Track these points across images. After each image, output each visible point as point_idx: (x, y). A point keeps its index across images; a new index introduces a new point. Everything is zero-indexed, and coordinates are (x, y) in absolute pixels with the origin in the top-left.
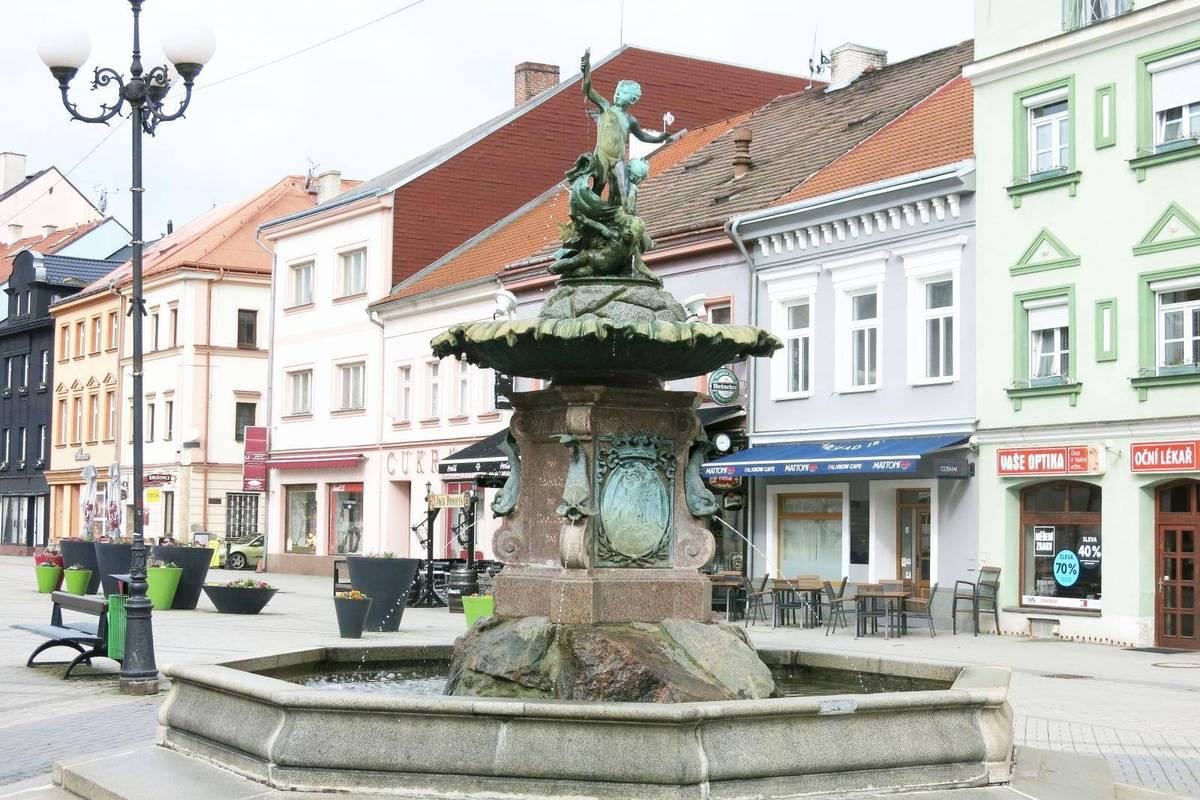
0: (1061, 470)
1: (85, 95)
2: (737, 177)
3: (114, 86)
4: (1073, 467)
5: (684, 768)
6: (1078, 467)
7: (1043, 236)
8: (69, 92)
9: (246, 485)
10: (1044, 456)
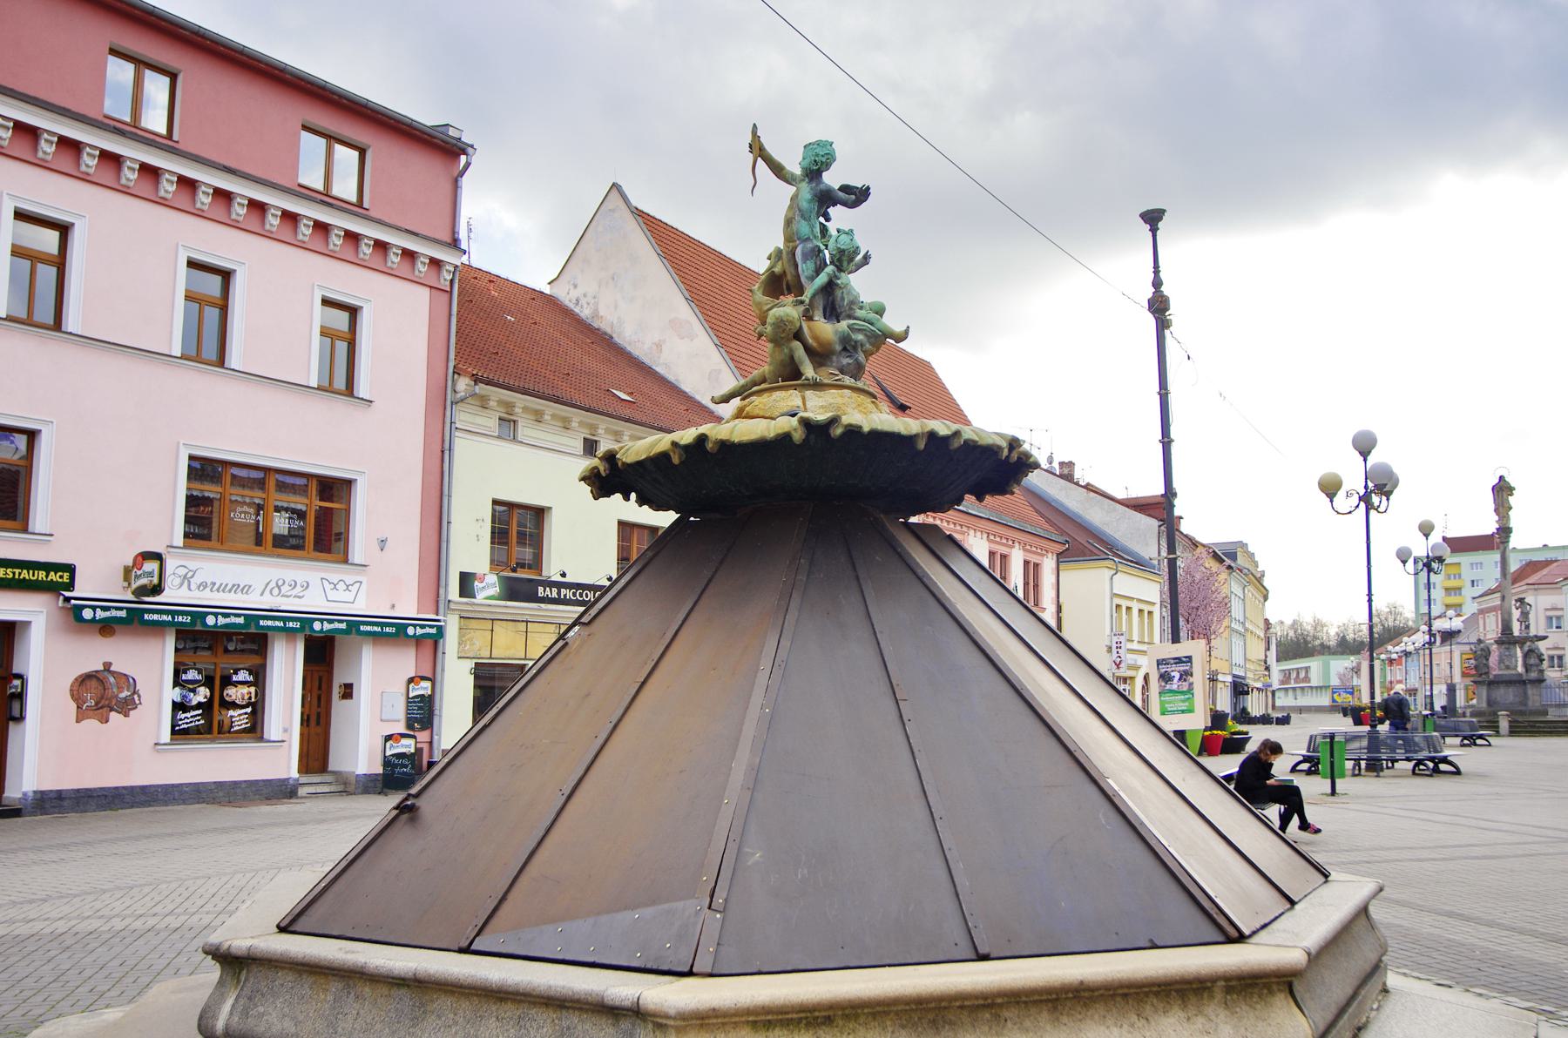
3: (1356, 497)
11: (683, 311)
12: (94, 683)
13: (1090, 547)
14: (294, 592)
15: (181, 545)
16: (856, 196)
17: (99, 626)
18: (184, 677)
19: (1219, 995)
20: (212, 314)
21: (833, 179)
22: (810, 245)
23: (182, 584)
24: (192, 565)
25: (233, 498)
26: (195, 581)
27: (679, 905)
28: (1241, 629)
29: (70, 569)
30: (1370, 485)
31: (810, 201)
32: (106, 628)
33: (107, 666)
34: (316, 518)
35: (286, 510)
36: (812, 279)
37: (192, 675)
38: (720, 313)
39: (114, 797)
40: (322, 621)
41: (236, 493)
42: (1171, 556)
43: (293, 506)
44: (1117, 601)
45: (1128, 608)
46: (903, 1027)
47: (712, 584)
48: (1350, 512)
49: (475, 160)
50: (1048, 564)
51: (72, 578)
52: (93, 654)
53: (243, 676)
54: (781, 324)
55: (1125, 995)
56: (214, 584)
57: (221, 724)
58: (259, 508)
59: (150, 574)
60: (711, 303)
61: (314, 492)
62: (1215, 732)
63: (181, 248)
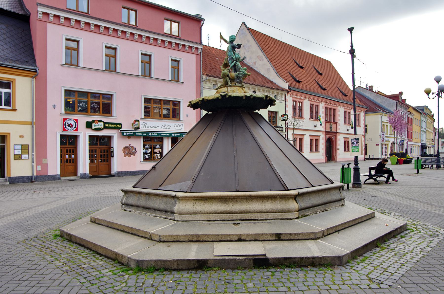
3: (435, 94)
11: (260, 53)
12: (127, 149)
13: (376, 109)
14: (168, 127)
15: (143, 118)
16: (239, 46)
17: (127, 136)
18: (146, 147)
19: (279, 199)
20: (147, 65)
21: (235, 43)
22: (231, 57)
23: (144, 127)
24: (146, 122)
25: (154, 107)
26: (147, 126)
27: (188, 181)
28: (425, 130)
29: (121, 124)
30: (439, 91)
31: (231, 48)
32: (129, 137)
33: (130, 145)
34: (172, 111)
35: (166, 109)
36: (231, 64)
37: (147, 147)
38: (271, 53)
39: (133, 173)
40: (174, 134)
41: (155, 105)
42: (355, 114)
43: (167, 108)
44: (383, 123)
45: (387, 126)
46: (219, 201)
47: (208, 126)
48: (433, 98)
49: (205, 22)
50: (362, 114)
51: (122, 126)
52: (127, 142)
53: (158, 146)
54: (224, 74)
55: (260, 198)
56: (151, 126)
57: (154, 157)
58: (160, 108)
59: (137, 125)
60: (268, 51)
61: (172, 104)
62: (401, 158)
63: (140, 51)
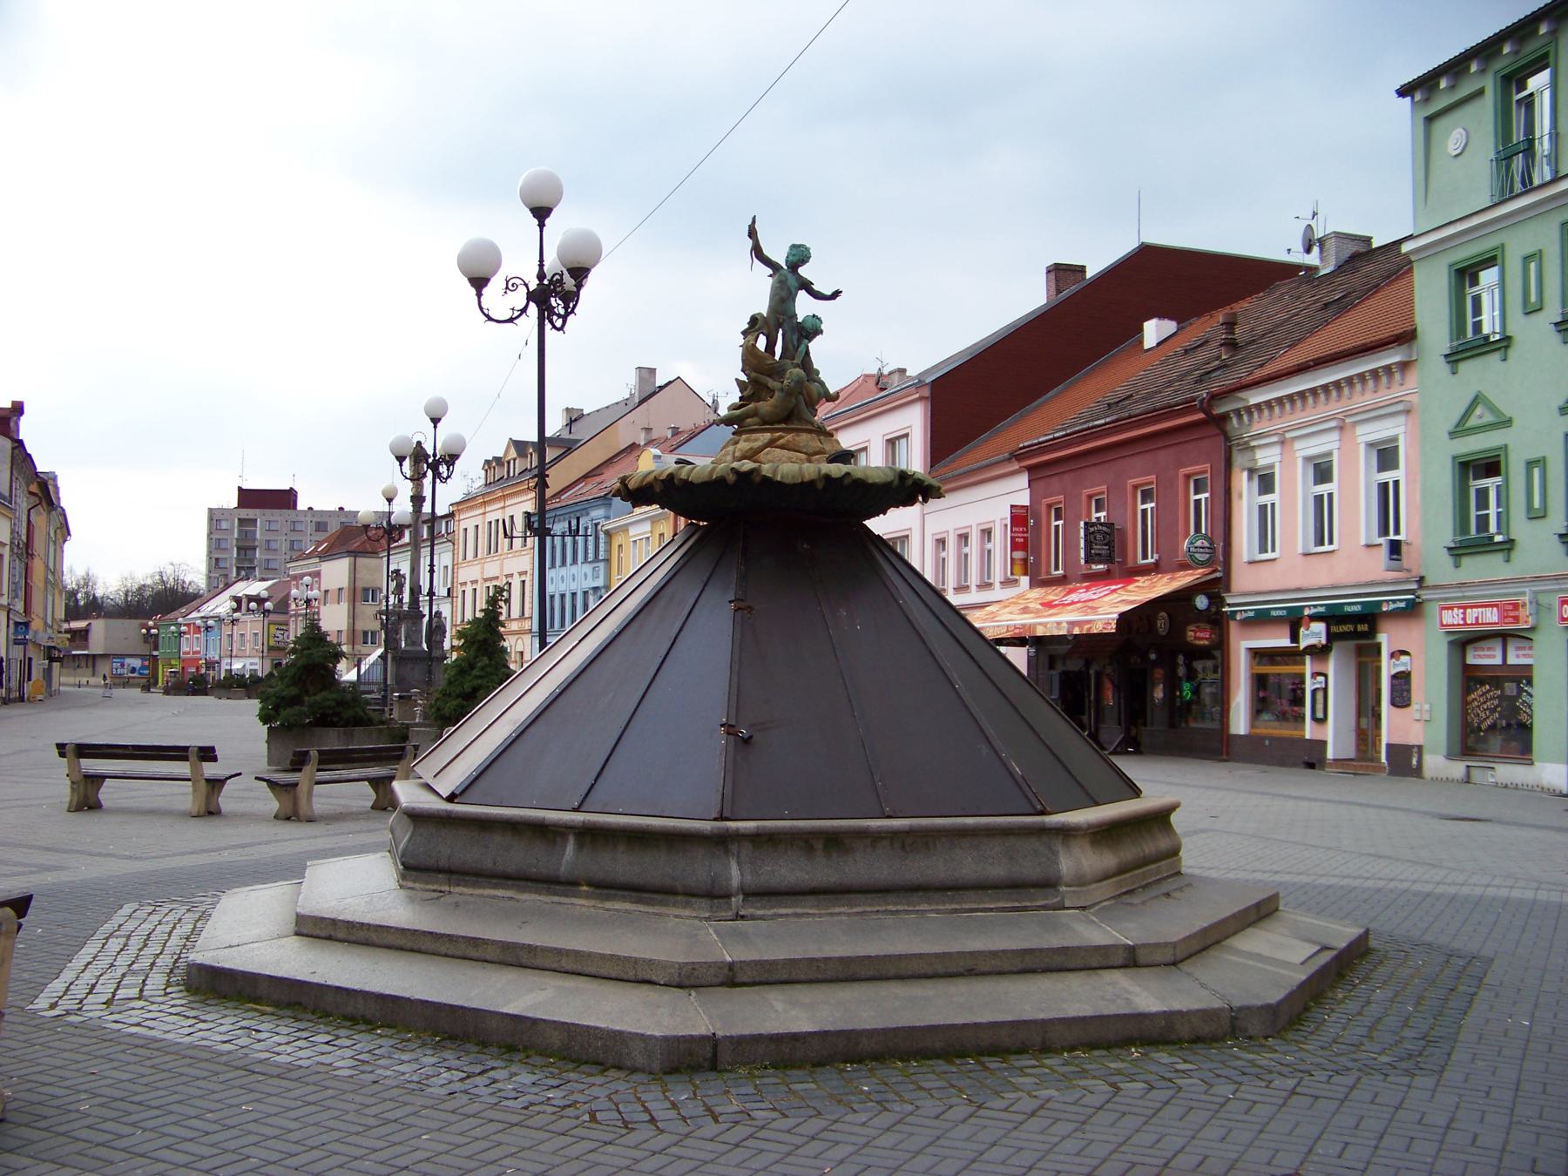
0: (1495, 623)
1: (498, 299)
2: (1224, 357)
3: (522, 291)
4: (1506, 621)
5: (713, 881)
6: (1511, 620)
7: (1477, 400)
8: (482, 299)
9: (353, 616)
10: (1480, 610)
